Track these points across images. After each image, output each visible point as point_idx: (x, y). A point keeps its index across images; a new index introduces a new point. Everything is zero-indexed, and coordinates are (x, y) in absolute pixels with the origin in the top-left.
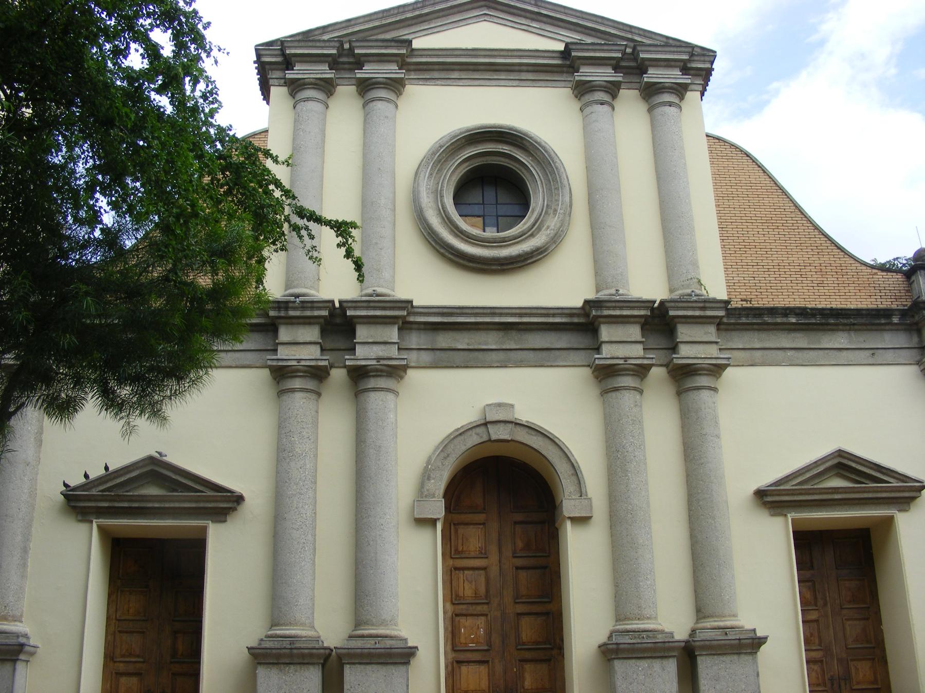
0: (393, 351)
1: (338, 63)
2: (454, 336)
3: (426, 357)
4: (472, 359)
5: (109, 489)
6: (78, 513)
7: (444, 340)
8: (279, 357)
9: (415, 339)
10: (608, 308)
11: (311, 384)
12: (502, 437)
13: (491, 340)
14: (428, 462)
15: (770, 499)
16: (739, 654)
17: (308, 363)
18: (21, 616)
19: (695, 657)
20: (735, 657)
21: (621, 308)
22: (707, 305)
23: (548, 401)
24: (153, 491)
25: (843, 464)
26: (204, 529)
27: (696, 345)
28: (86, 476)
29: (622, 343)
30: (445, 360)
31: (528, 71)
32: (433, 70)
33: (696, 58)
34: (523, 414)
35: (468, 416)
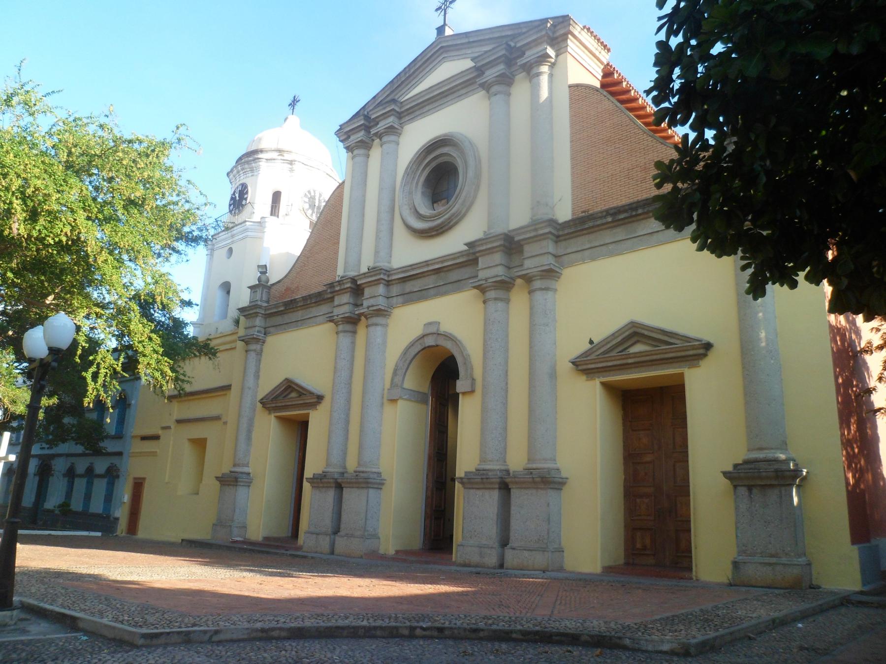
0: (550, 260)
1: (557, 38)
2: (417, 282)
3: (400, 299)
4: (422, 295)
5: (604, 353)
6: (586, 374)
7: (409, 286)
8: (479, 278)
9: (395, 290)
10: (479, 246)
11: (500, 294)
12: (431, 344)
13: (430, 281)
14: (396, 366)
15: (585, 366)
16: (537, 488)
17: (494, 280)
18: (248, 463)
19: (510, 489)
20: (534, 491)
21: (486, 244)
22: (537, 227)
23: (455, 315)
24: (639, 348)
25: (636, 333)
26: (681, 375)
27: (375, 296)
28: (591, 342)
29: (492, 267)
30: (410, 298)
31: (462, 88)
32: (458, 90)
33: (558, 27)
34: (445, 328)
35: (417, 331)
